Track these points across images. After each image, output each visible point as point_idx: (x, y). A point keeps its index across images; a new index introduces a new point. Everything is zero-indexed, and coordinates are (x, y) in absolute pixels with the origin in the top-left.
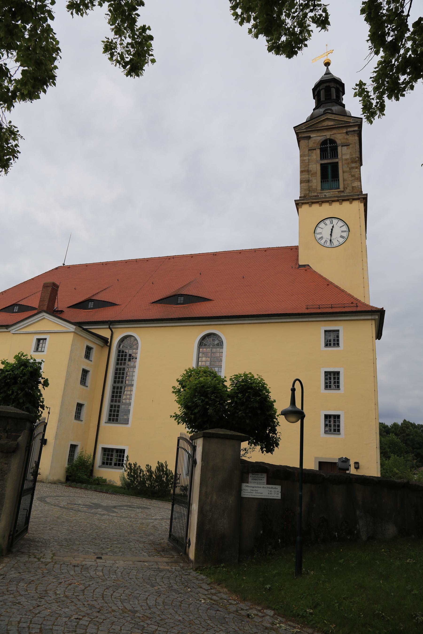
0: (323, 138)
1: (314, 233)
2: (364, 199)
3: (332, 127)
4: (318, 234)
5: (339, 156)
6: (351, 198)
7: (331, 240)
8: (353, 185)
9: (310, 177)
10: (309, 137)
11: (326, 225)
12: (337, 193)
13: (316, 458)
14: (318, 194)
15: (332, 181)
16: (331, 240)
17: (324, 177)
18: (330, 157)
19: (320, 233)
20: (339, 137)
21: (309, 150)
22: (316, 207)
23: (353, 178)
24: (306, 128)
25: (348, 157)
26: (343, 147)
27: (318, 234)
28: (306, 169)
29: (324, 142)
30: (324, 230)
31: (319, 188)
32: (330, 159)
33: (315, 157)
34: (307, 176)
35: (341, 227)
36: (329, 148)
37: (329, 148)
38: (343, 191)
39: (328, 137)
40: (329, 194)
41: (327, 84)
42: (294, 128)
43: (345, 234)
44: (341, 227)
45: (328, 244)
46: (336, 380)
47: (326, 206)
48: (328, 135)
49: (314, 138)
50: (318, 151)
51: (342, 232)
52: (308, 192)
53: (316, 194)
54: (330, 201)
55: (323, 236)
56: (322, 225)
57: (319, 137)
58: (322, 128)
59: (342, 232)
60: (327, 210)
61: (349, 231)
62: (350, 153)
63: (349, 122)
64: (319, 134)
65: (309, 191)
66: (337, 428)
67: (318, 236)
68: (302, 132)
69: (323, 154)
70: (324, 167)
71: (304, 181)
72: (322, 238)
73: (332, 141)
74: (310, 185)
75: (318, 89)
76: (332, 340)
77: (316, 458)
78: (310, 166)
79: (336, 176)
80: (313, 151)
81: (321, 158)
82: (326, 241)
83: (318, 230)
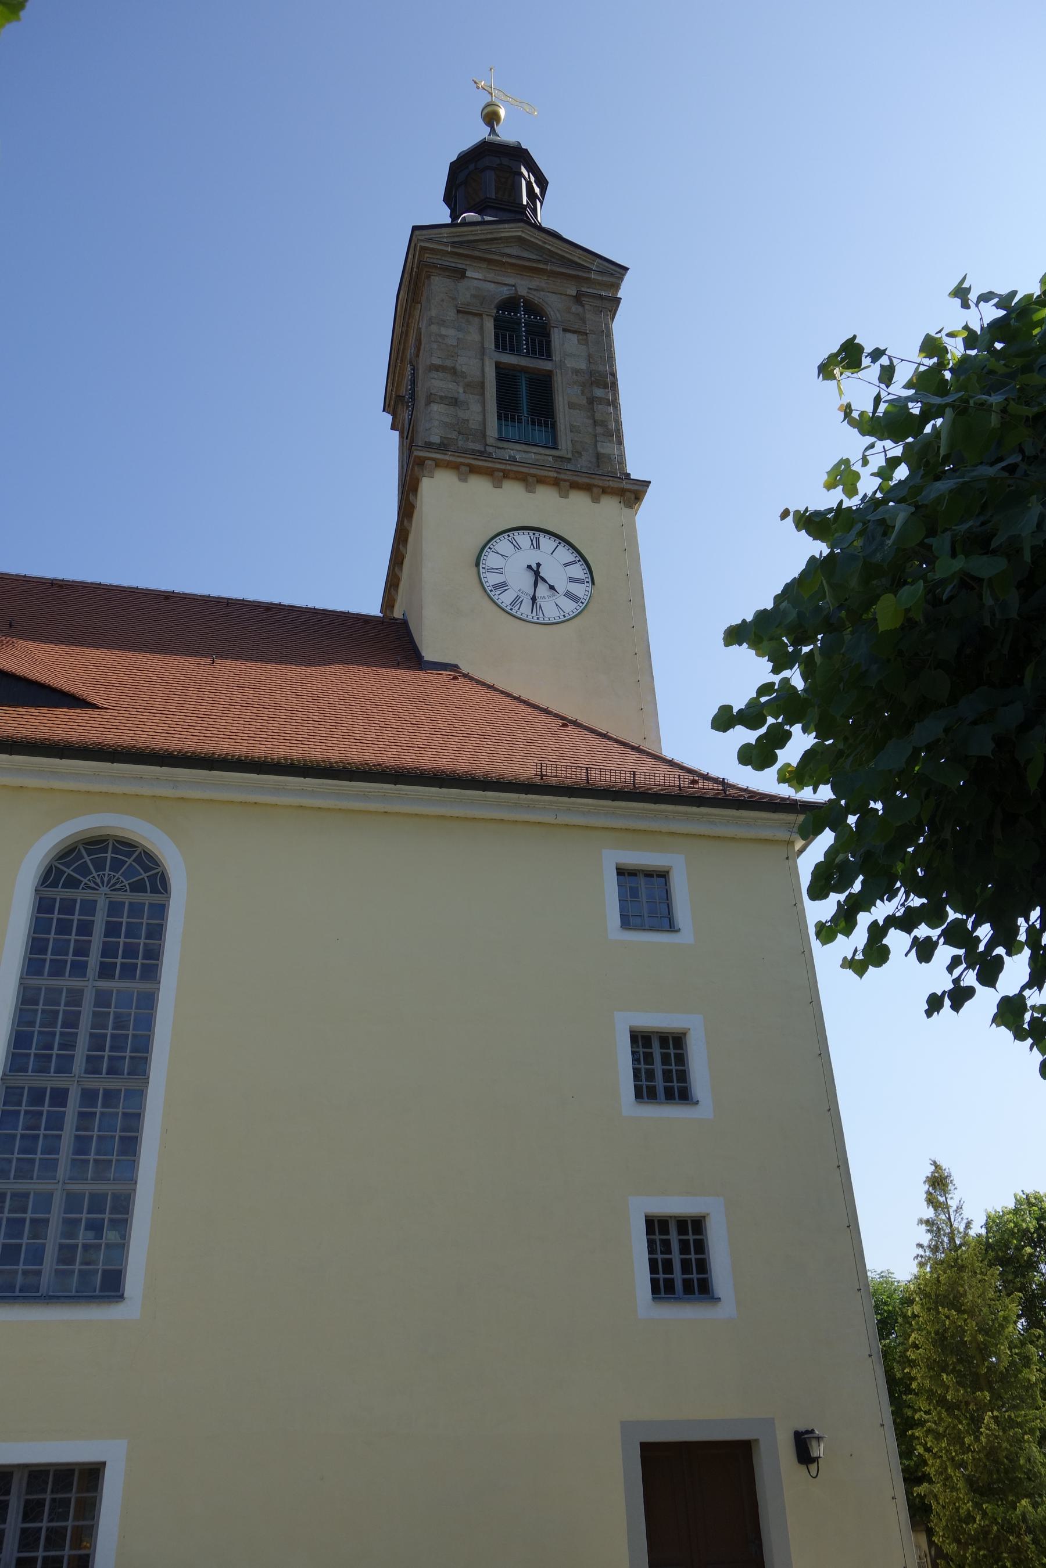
0: (505, 292)
1: (477, 565)
2: (633, 492)
3: (535, 265)
4: (491, 570)
5: (557, 356)
6: (600, 483)
7: (534, 599)
8: (601, 450)
9: (461, 390)
10: (461, 274)
11: (518, 547)
12: (550, 459)
13: (626, 1427)
14: (490, 449)
15: (533, 424)
16: (534, 599)
17: (507, 407)
18: (528, 352)
19: (499, 571)
20: (555, 303)
21: (458, 311)
22: (479, 486)
23: (599, 430)
24: (453, 244)
25: (583, 365)
26: (569, 335)
27: (491, 570)
28: (449, 363)
29: (510, 304)
30: (511, 562)
31: (492, 430)
32: (527, 355)
33: (477, 337)
34: (452, 386)
35: (566, 565)
36: (521, 327)
37: (521, 327)
38: (569, 460)
39: (523, 292)
40: (524, 455)
41: (505, 161)
42: (415, 228)
43: (579, 590)
44: (566, 565)
45: (525, 609)
46: (674, 1067)
47: (513, 491)
48: (523, 286)
49: (475, 283)
50: (489, 325)
51: (572, 580)
52: (454, 435)
53: (478, 447)
54: (530, 480)
55: (509, 582)
56: (503, 545)
57: (493, 285)
58: (505, 259)
59: (572, 580)
60: (514, 502)
61: (593, 583)
62: (589, 356)
63: (590, 270)
64: (491, 276)
65: (459, 433)
66: (695, 1276)
67: (492, 579)
68: (427, 261)
69: (506, 336)
70: (505, 377)
71: (441, 397)
72: (502, 586)
73: (533, 309)
74: (461, 414)
75: (472, 167)
76: (646, 900)
77: (626, 1427)
78: (461, 360)
79: (543, 411)
80: (471, 318)
81: (497, 346)
82: (517, 601)
83: (491, 560)
